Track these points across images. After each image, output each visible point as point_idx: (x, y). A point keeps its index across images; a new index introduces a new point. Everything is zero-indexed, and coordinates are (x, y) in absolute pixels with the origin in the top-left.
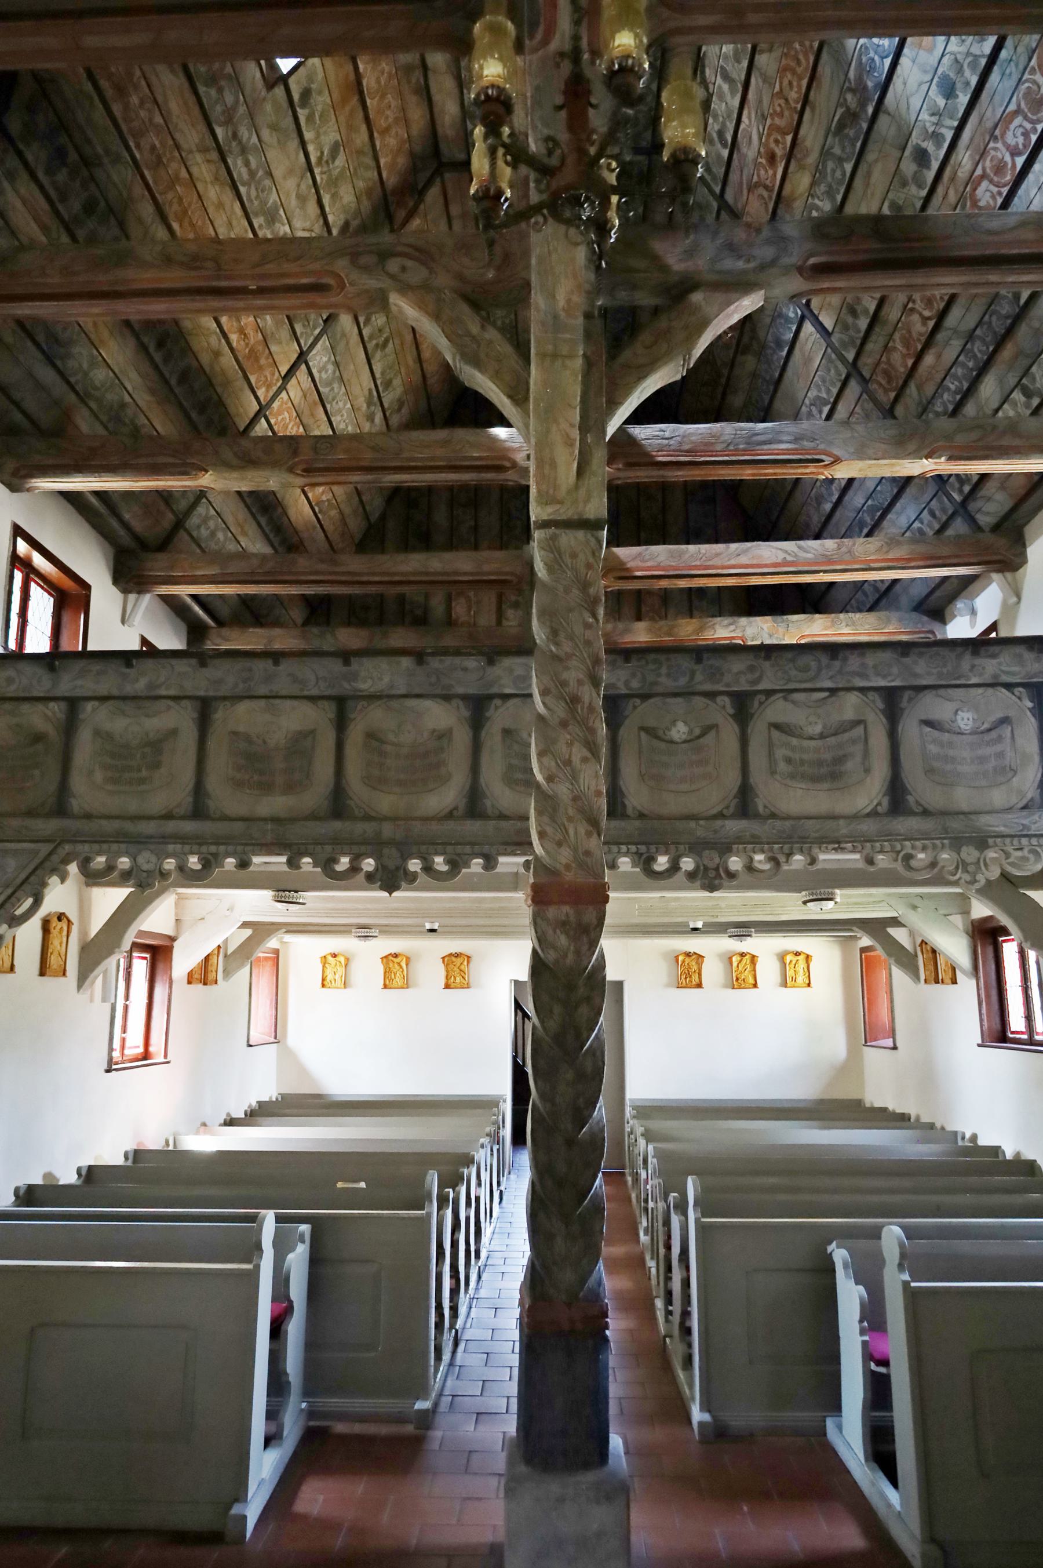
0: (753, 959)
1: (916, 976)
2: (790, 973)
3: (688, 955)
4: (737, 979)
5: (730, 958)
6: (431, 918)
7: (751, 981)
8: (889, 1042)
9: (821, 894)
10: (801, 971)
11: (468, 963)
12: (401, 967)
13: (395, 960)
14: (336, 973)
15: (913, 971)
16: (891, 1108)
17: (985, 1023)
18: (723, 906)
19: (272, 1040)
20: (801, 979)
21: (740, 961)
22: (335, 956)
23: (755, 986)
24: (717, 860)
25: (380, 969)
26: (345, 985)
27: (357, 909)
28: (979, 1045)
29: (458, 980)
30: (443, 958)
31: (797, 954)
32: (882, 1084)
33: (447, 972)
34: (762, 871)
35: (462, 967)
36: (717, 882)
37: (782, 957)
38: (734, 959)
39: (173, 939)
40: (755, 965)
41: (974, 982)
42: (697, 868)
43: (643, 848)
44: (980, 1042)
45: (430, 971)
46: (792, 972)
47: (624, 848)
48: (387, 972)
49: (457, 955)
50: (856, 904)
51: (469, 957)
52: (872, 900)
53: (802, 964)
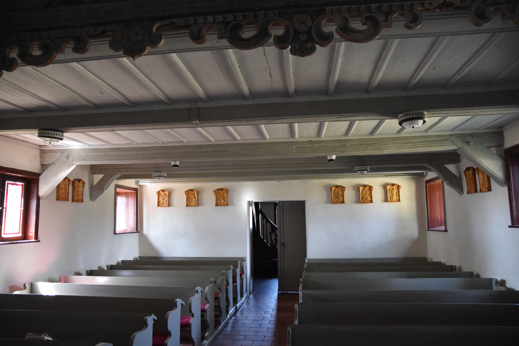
0: (371, 188)
1: (460, 190)
2: (389, 195)
3: (337, 187)
4: (362, 198)
5: (359, 188)
6: (175, 159)
7: (369, 199)
8: (443, 228)
9: (413, 114)
10: (395, 194)
11: (227, 193)
12: (195, 196)
13: (192, 193)
14: (165, 199)
15: (459, 188)
16: (443, 262)
17: (515, 213)
18: (348, 145)
19: (135, 231)
20: (395, 198)
21: (364, 189)
22: (163, 191)
23: (371, 201)
24: (309, 23)
25: (185, 197)
26: (169, 205)
27: (132, 155)
28: (510, 227)
29: (222, 201)
30: (214, 191)
31: (393, 185)
32: (439, 248)
33: (217, 198)
34: (358, 32)
35: (224, 195)
36: (309, 45)
37: (385, 186)
38: (361, 188)
39: (39, 175)
40: (371, 191)
41: (506, 189)
42: (287, 31)
43: (230, 17)
44: (510, 224)
45: (209, 198)
46: (390, 194)
47: (210, 18)
48: (188, 199)
49: (221, 190)
50: (430, 141)
51: (227, 190)
52: (441, 139)
53: (395, 191)
